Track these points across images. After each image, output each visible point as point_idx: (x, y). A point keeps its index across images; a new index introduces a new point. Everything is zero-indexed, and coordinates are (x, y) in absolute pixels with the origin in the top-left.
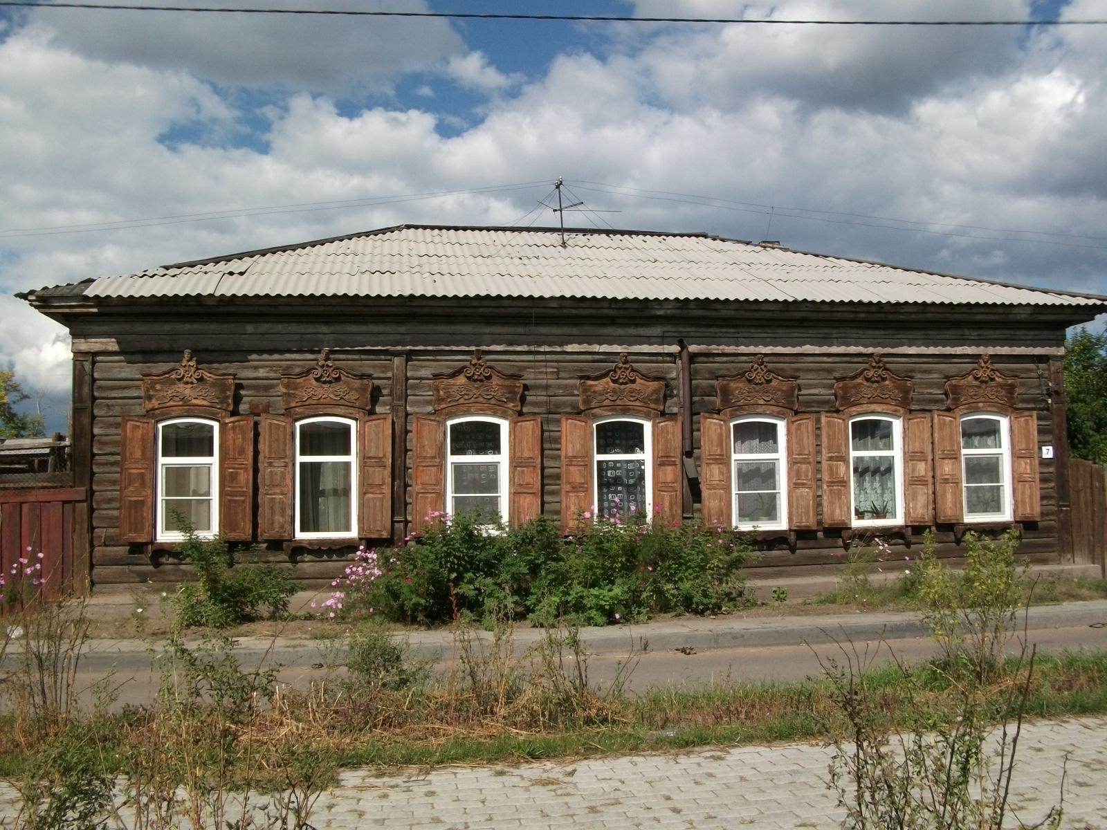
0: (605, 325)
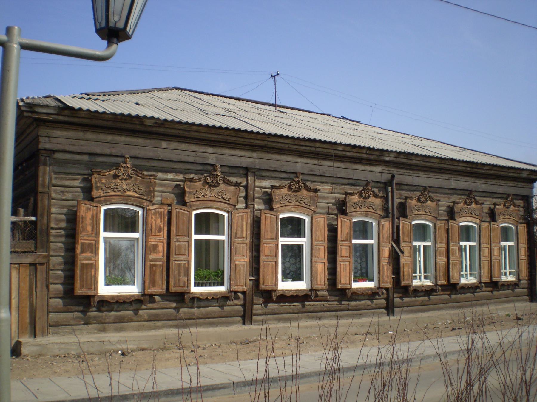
0: (355, 163)
